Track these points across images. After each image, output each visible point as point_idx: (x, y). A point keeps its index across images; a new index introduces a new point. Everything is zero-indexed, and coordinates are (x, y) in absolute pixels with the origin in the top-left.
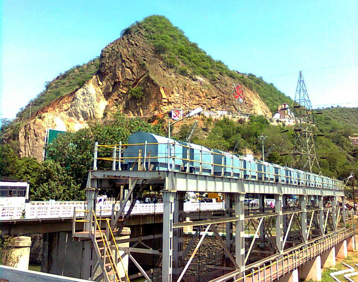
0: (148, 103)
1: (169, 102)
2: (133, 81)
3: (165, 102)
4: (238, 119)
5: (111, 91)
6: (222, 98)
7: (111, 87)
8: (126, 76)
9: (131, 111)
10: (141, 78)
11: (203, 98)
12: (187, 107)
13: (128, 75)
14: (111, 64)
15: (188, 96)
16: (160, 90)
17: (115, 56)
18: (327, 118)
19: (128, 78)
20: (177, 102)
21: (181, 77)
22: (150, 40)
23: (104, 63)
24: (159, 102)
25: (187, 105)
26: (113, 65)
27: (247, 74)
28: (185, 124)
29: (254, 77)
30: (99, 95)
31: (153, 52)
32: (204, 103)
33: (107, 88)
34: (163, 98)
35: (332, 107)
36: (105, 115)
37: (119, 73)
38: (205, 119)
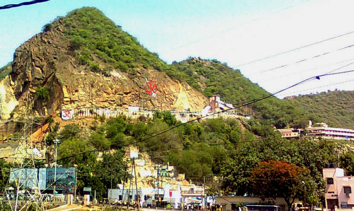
0: (52, 103)
1: (71, 100)
2: (42, 80)
3: (67, 101)
4: (139, 116)
5: (21, 91)
6: (137, 93)
7: (21, 86)
8: (35, 76)
9: (37, 111)
10: (50, 76)
11: (111, 95)
12: (93, 104)
13: (38, 74)
14: (22, 64)
15: (95, 94)
16: (62, 88)
17: (26, 56)
18: (290, 107)
19: (37, 77)
20: (82, 101)
21: (91, 74)
22: (68, 36)
23: (16, 63)
24: (61, 102)
25: (94, 103)
26: (25, 64)
27: (210, 60)
28: (73, 124)
29: (217, 63)
30: (10, 95)
31: (67, 48)
32: (112, 100)
33: (18, 88)
34: (65, 96)
35: (329, 91)
36: (12, 115)
37: (29, 72)
38: (98, 117)
